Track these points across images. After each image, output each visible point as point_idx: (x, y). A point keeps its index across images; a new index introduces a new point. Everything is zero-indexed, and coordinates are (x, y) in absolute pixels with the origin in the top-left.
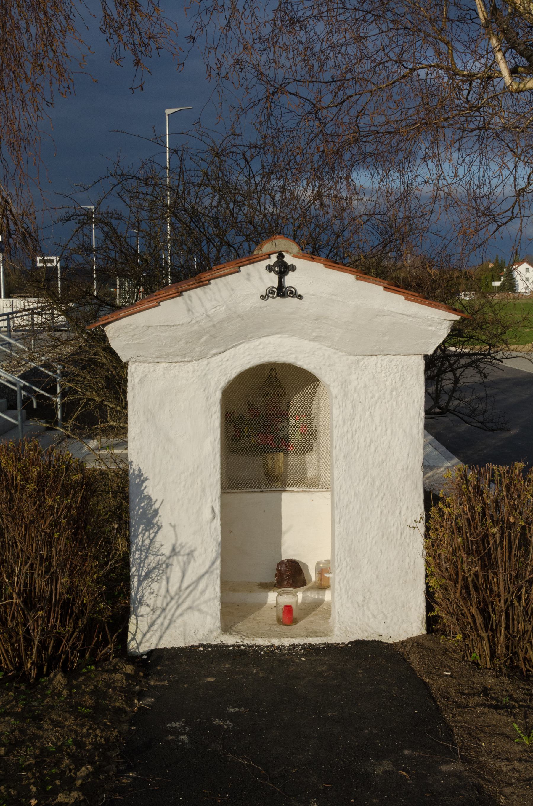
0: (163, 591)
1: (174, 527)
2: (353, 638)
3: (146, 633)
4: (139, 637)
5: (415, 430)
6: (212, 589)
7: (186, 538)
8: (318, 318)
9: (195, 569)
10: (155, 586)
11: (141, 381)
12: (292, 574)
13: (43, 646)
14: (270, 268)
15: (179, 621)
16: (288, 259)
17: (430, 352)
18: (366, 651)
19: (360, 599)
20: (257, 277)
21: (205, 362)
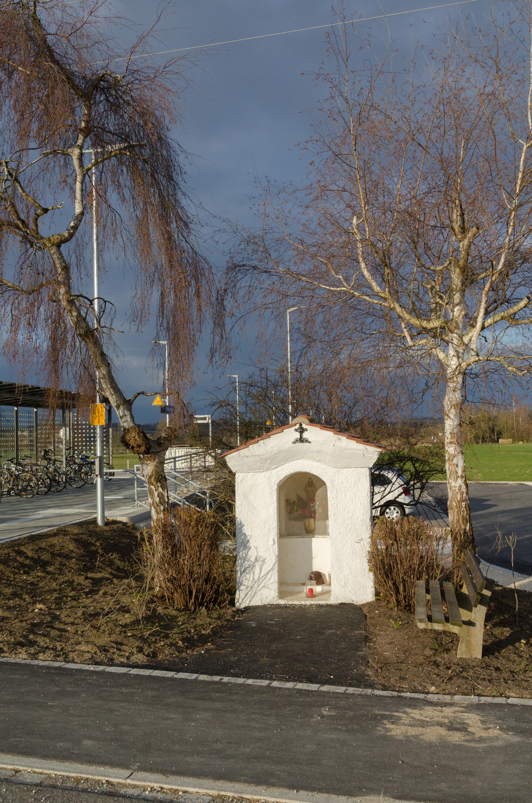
0: (251, 579)
1: (256, 548)
2: (340, 602)
3: (244, 599)
4: (240, 600)
5: (366, 502)
6: (274, 578)
7: (262, 553)
8: (318, 452)
9: (267, 567)
10: (248, 576)
11: (241, 481)
12: (318, 578)
13: (197, 598)
14: (296, 430)
15: (259, 593)
16: (304, 426)
17: (371, 466)
18: (345, 607)
19: (343, 583)
20: (290, 434)
21: (269, 472)
